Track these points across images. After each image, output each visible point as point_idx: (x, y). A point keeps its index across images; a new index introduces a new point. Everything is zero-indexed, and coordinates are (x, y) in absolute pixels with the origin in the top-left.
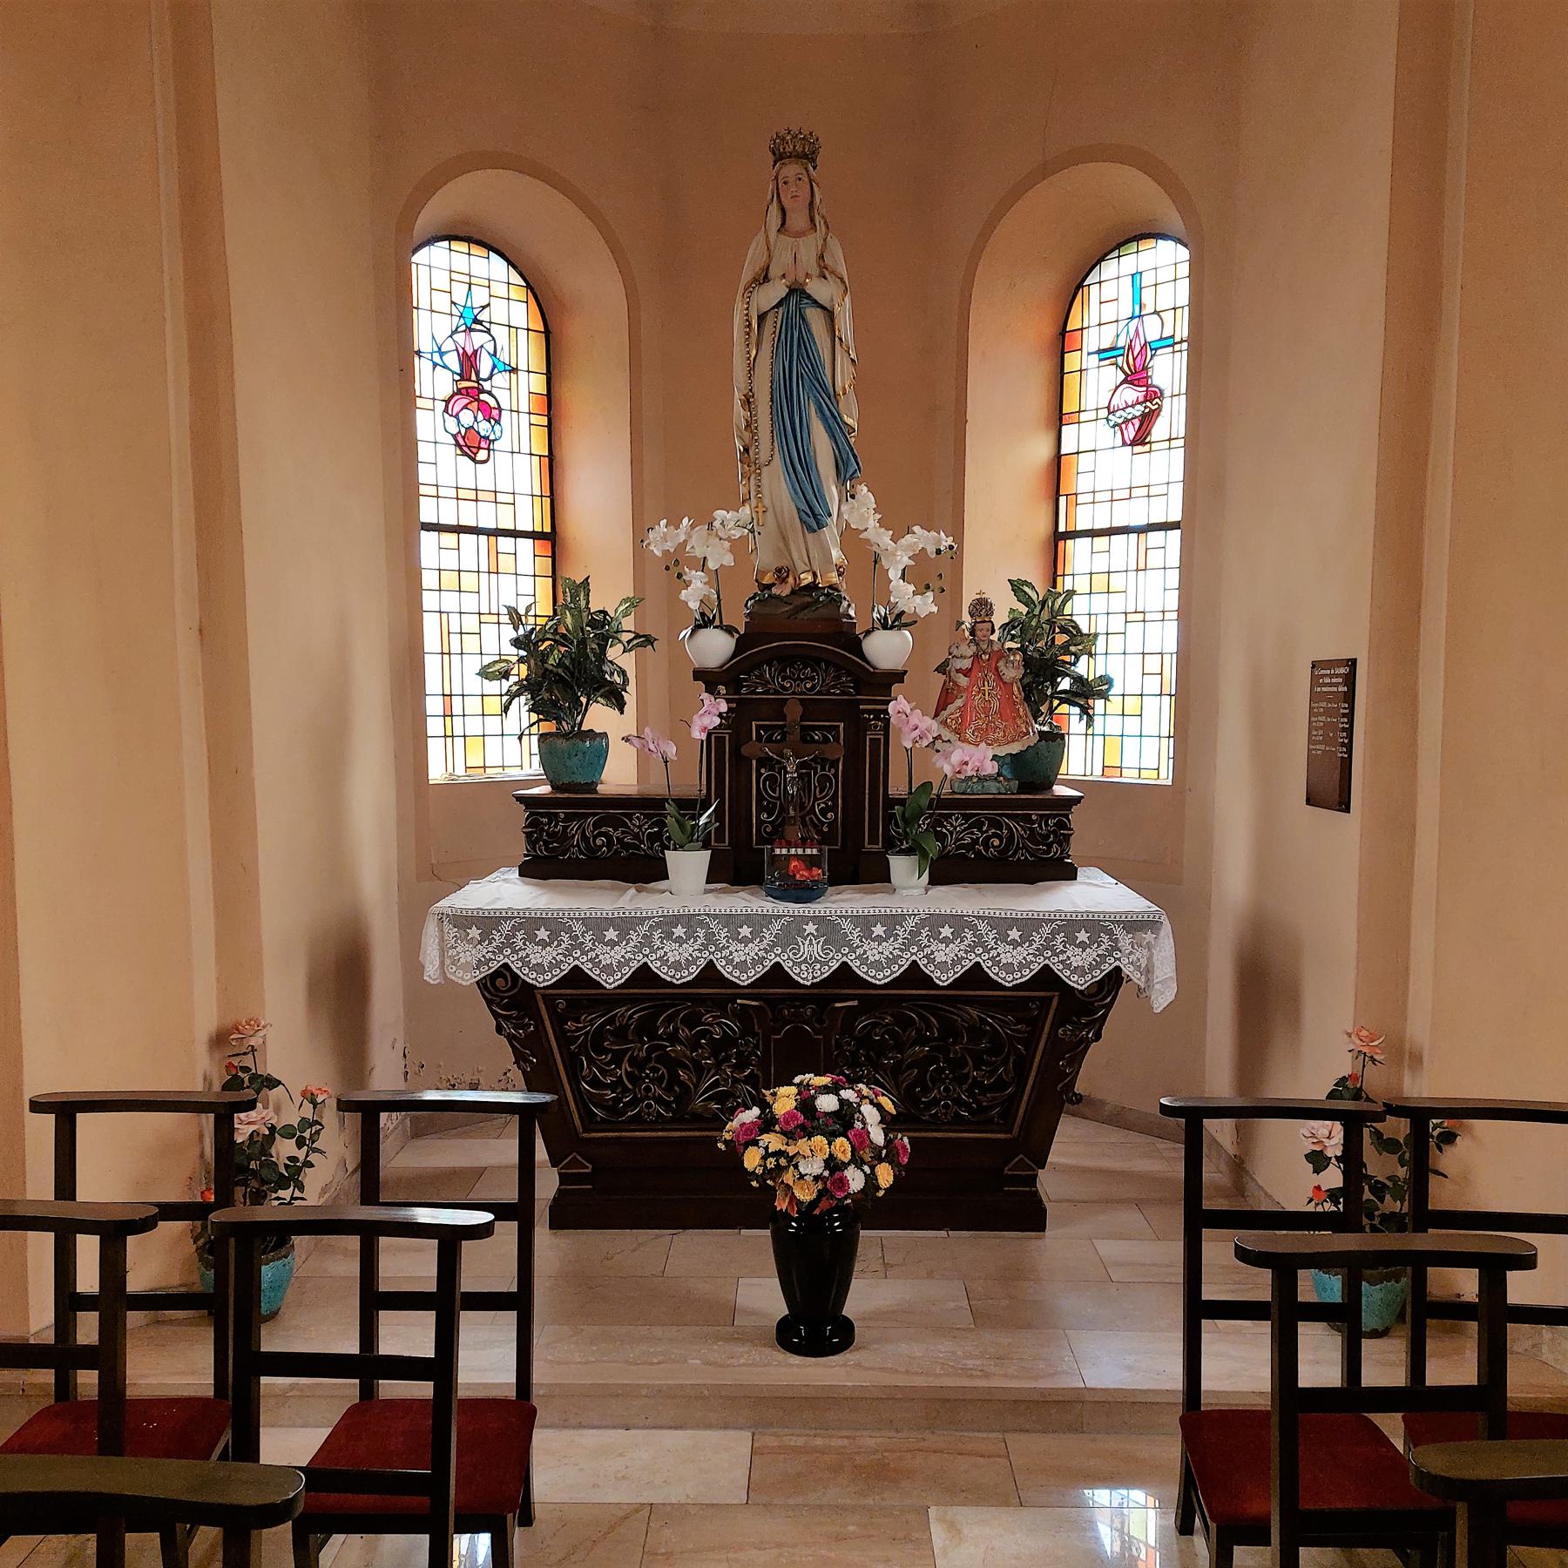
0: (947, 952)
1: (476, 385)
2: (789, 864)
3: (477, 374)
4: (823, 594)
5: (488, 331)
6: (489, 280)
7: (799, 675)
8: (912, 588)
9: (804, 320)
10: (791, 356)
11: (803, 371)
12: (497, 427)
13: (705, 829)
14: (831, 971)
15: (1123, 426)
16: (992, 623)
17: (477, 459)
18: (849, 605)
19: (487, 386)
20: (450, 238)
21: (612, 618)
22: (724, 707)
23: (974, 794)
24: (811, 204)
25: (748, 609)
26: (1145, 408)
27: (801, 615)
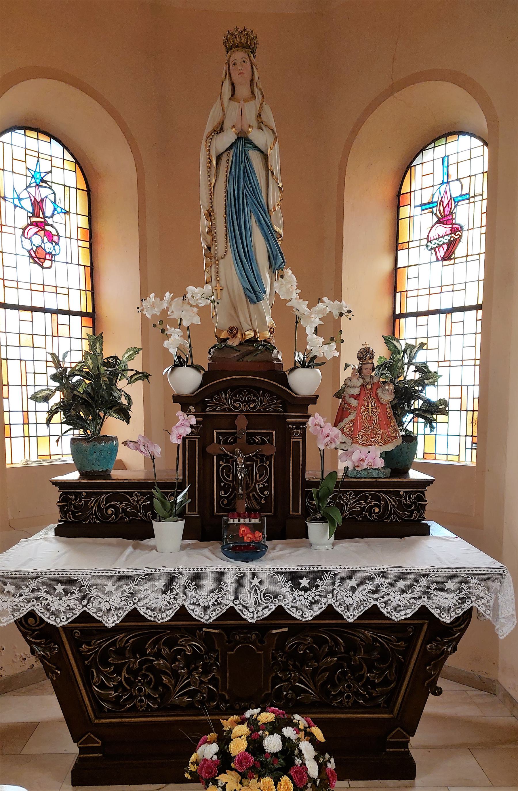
0: (353, 597)
1: (43, 220)
2: (239, 529)
3: (44, 213)
4: (261, 345)
5: (51, 188)
6: (51, 156)
7: (245, 399)
8: (321, 340)
9: (247, 158)
10: (239, 183)
11: (247, 193)
12: (57, 247)
13: (181, 505)
14: (270, 612)
15: (437, 249)
16: (373, 364)
17: (44, 266)
18: (278, 352)
19: (50, 221)
20: (26, 128)
21: (121, 361)
22: (193, 421)
23: (362, 478)
24: (252, 81)
25: (210, 355)
26: (451, 237)
27: (247, 359)
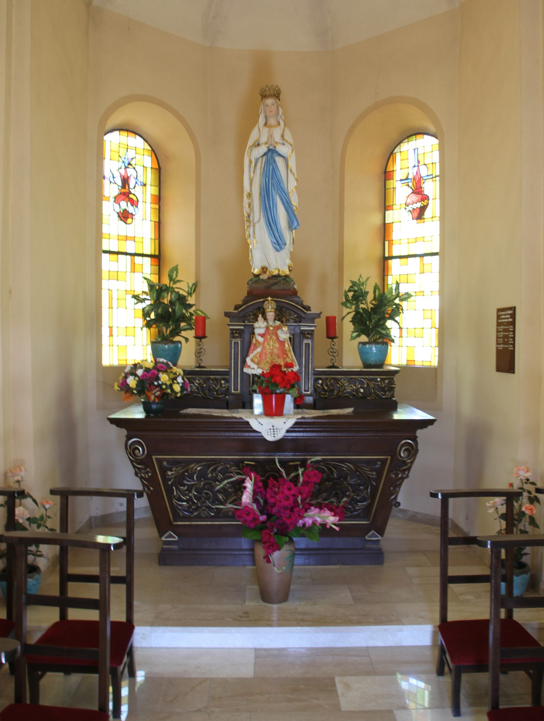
19: (132, 191)
26: (422, 204)
